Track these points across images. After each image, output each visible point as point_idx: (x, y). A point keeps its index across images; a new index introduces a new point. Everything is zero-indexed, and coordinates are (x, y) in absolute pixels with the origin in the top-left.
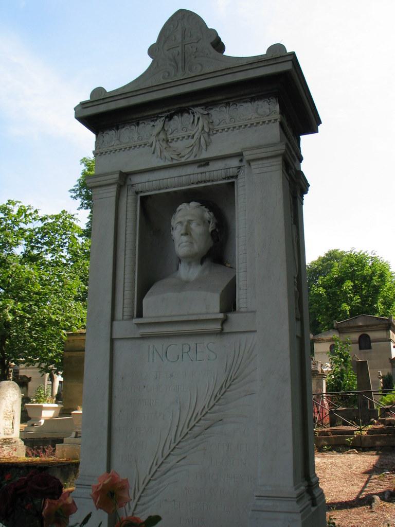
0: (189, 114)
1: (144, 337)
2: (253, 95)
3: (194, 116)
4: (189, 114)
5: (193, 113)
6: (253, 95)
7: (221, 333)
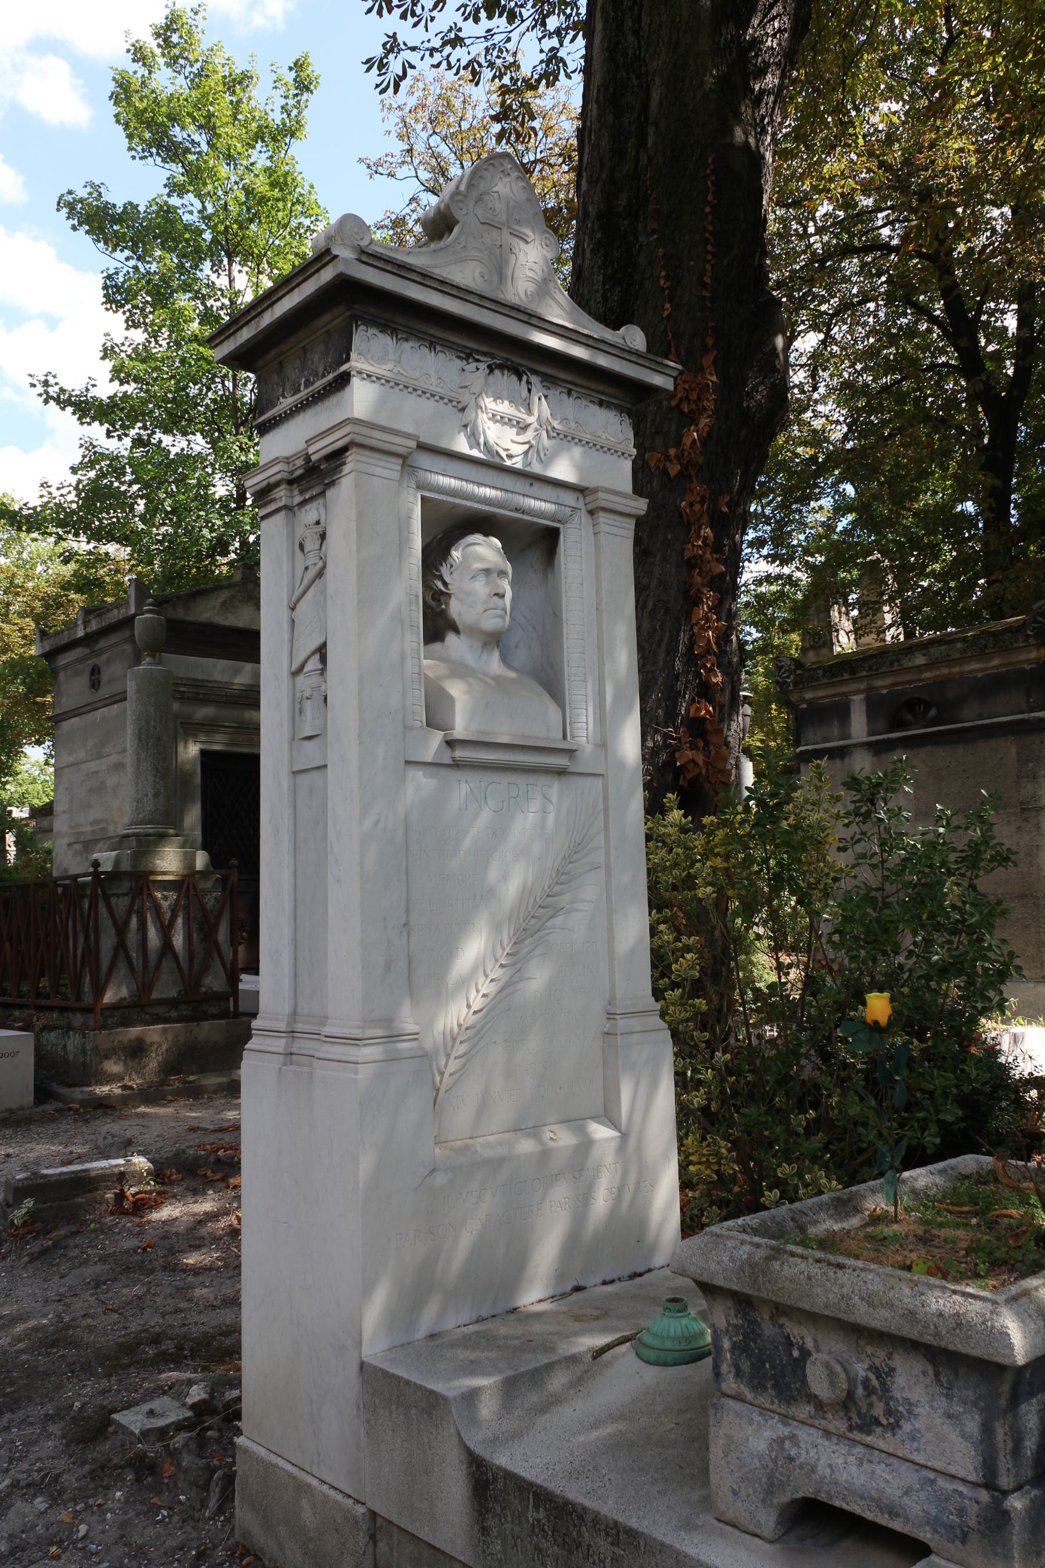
0: (520, 379)
1: (456, 765)
2: (603, 398)
3: (529, 391)
4: (520, 379)
5: (528, 383)
6: (603, 398)
7: (561, 773)
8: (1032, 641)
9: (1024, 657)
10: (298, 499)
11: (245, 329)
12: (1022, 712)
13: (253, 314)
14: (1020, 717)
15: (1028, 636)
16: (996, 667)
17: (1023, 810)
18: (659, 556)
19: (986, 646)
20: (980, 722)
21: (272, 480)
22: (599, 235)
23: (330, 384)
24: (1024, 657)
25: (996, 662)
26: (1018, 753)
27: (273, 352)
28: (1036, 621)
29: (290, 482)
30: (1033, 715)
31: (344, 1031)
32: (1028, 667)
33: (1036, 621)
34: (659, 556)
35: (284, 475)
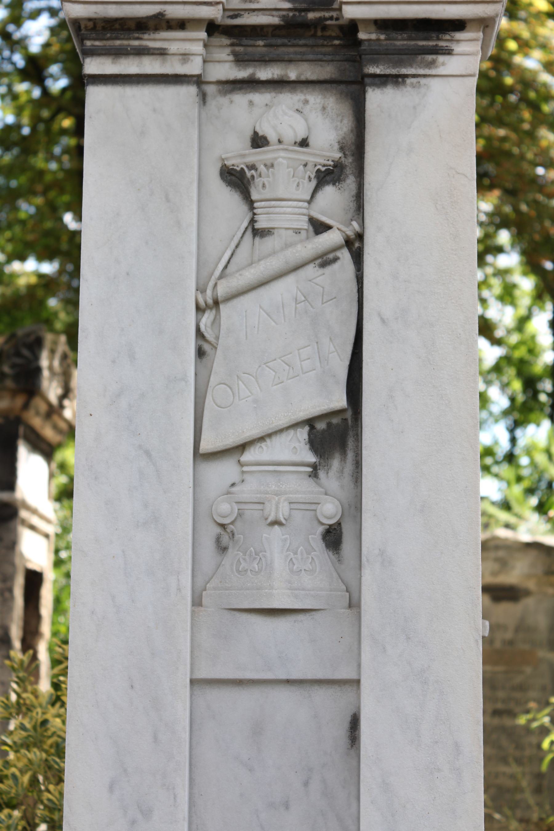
28: (18, 354)
29: (212, 28)
33: (18, 354)
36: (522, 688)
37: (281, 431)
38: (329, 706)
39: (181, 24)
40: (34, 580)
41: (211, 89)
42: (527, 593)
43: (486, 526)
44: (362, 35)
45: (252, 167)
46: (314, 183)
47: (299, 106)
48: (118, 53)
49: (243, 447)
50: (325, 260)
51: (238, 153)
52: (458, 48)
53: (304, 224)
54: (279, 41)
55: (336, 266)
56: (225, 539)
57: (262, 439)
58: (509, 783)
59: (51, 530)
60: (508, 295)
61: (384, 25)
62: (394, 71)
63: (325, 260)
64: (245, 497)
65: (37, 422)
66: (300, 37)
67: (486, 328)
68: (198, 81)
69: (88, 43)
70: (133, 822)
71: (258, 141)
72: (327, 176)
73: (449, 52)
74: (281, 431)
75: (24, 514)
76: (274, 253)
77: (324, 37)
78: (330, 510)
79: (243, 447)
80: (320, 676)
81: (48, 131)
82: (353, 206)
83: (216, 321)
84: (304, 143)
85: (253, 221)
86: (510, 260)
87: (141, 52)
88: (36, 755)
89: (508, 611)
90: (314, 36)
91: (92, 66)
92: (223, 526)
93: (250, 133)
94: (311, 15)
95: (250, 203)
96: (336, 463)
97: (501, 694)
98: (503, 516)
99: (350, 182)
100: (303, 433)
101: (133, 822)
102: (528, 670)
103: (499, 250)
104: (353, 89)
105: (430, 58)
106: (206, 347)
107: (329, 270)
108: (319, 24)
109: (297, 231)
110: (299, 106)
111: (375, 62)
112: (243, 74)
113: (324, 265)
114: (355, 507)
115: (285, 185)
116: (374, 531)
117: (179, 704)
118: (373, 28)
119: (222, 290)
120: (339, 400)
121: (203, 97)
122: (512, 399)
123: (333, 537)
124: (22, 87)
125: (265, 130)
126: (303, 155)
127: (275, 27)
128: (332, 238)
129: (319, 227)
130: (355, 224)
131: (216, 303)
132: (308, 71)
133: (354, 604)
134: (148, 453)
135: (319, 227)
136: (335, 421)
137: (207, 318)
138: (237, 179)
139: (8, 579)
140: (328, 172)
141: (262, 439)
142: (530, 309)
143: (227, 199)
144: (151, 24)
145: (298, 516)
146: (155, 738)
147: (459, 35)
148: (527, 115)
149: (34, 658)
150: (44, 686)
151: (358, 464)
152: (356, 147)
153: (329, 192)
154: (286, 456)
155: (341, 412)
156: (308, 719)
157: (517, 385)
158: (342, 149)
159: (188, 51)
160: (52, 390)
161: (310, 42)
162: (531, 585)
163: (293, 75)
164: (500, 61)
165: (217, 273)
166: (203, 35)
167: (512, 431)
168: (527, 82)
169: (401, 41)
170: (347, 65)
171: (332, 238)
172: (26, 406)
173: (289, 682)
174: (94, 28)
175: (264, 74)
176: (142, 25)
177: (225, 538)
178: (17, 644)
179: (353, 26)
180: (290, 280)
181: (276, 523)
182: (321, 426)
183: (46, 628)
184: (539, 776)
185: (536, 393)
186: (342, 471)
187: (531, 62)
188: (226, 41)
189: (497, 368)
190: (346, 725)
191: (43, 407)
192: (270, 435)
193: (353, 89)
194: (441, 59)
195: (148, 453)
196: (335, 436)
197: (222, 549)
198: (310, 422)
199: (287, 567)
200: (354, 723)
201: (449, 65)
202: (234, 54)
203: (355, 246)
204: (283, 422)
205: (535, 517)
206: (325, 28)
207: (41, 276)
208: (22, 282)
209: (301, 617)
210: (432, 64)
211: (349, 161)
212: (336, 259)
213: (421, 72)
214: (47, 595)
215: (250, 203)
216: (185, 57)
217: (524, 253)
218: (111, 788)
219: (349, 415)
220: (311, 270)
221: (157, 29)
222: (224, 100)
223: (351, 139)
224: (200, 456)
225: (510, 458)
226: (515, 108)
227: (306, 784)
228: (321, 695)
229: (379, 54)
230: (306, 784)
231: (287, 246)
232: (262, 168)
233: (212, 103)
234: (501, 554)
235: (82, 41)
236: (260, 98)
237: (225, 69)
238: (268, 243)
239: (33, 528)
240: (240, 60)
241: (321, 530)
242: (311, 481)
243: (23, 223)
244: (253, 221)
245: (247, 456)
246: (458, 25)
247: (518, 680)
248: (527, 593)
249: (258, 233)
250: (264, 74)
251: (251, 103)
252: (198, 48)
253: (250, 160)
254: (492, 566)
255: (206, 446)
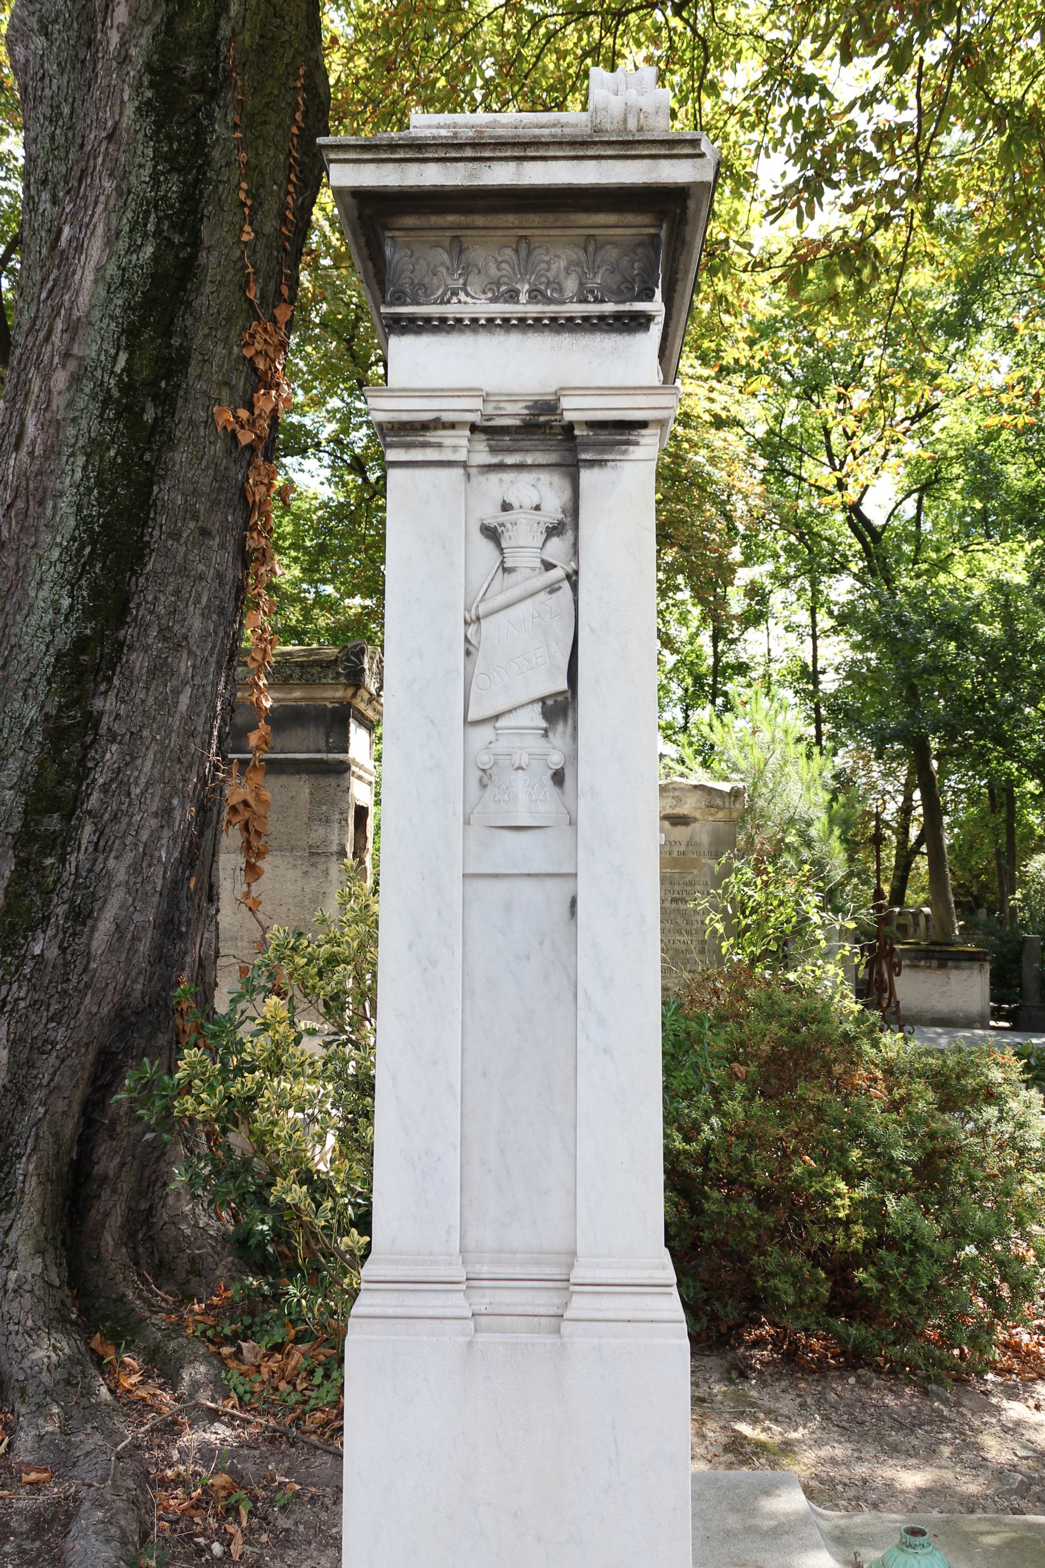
8: (343, 680)
9: (329, 694)
10: (484, 457)
11: (432, 167)
12: (319, 751)
13: (469, 153)
14: (318, 756)
15: (338, 673)
16: (295, 700)
17: (312, 854)
18: (217, 540)
19: (291, 676)
20: (273, 756)
21: (447, 417)
22: (149, 94)
23: (602, 318)
24: (329, 694)
25: (297, 694)
26: (311, 793)
27: (451, 219)
28: (349, 660)
29: (474, 428)
30: (332, 756)
31: (511, 1270)
32: (330, 706)
33: (349, 660)
34: (217, 540)
35: (475, 418)
36: (691, 884)
37: (523, 706)
38: (558, 891)
39: (453, 426)
40: (361, 813)
41: (473, 471)
42: (695, 820)
43: (668, 776)
44: (577, 432)
45: (502, 525)
46: (545, 535)
47: (534, 482)
48: (409, 446)
49: (497, 717)
50: (552, 589)
51: (492, 515)
52: (643, 441)
53: (539, 565)
54: (520, 437)
55: (560, 593)
56: (486, 779)
57: (510, 711)
58: (683, 947)
59: (372, 779)
60: (683, 620)
61: (592, 425)
62: (599, 457)
63: (552, 589)
64: (499, 751)
65: (362, 706)
66: (535, 434)
67: (667, 641)
68: (464, 465)
69: (388, 439)
70: (425, 970)
71: (506, 507)
72: (554, 531)
73: (637, 444)
74: (523, 706)
75: (353, 768)
76: (517, 584)
77: (551, 434)
78: (556, 760)
79: (497, 717)
80: (551, 871)
81: (368, 507)
82: (571, 551)
83: (478, 631)
84: (537, 508)
85: (503, 562)
86: (685, 595)
87: (425, 445)
88: (362, 928)
89: (681, 833)
90: (544, 433)
91: (392, 455)
92: (484, 771)
93: (500, 502)
94: (542, 419)
95: (501, 550)
96: (560, 727)
97: (677, 888)
98: (680, 768)
99: (569, 535)
100: (538, 707)
101: (425, 970)
102: (695, 871)
103: (677, 588)
104: (571, 469)
105: (624, 447)
106: (471, 649)
107: (555, 595)
108: (547, 425)
109: (533, 569)
110: (534, 482)
111: (585, 451)
112: (495, 460)
113: (551, 592)
114: (573, 757)
115: (525, 537)
116: (586, 773)
117: (455, 890)
118: (584, 427)
119: (481, 611)
120: (563, 685)
121: (468, 476)
122: (686, 690)
123: (558, 778)
124: (349, 478)
125: (511, 499)
126: (536, 516)
127: (518, 427)
128: (557, 573)
129: (548, 566)
130: (573, 564)
131: (478, 619)
132: (540, 458)
133: (573, 823)
134: (432, 722)
135: (548, 566)
136: (560, 699)
137: (472, 629)
138: (492, 533)
139: (343, 812)
140: (554, 528)
141: (510, 711)
142: (698, 628)
143: (486, 547)
144: (432, 425)
145: (534, 763)
146: (440, 914)
147: (643, 432)
148: (696, 493)
149: (362, 862)
150: (369, 883)
151: (575, 728)
152: (574, 510)
153: (555, 541)
154: (527, 723)
155: (564, 692)
156: (541, 901)
157: (689, 681)
158: (563, 512)
159: (457, 444)
160: (372, 685)
161: (542, 437)
162: (698, 815)
163: (529, 461)
164: (678, 458)
165: (479, 598)
166: (468, 433)
167: (686, 711)
168: (697, 472)
169: (604, 436)
170: (567, 453)
171: (557, 573)
172: (354, 695)
173: (529, 875)
174: (392, 429)
175: (510, 460)
176: (425, 426)
177: (485, 778)
178: (350, 855)
179: (570, 426)
180: (529, 602)
181: (520, 768)
182: (550, 702)
183: (370, 845)
184: (703, 942)
185: (702, 687)
186: (564, 733)
187: (700, 457)
188: (483, 437)
189: (675, 669)
190: (568, 904)
191: (366, 696)
192: (515, 709)
193: (571, 469)
194: (631, 448)
195: (432, 722)
196: (559, 709)
197: (484, 786)
198: (543, 700)
199: (527, 797)
200: (574, 902)
201: (635, 452)
202: (489, 446)
203: (573, 579)
204: (525, 699)
205: (701, 770)
206: (551, 427)
207: (364, 608)
208: (352, 612)
209: (537, 831)
210: (625, 452)
211: (568, 520)
212: (560, 588)
213: (618, 457)
214: (371, 823)
215: (501, 550)
216: (455, 448)
217: (692, 589)
218: (410, 947)
219: (569, 695)
220: (543, 596)
221: (435, 429)
222: (482, 479)
223: (570, 505)
224: (468, 723)
225: (685, 729)
226: (688, 490)
227: (541, 943)
228: (551, 884)
229: (589, 445)
230: (541, 943)
231: (526, 579)
232: (509, 525)
233: (474, 480)
234: (677, 793)
235: (384, 438)
236: (507, 477)
237: (484, 457)
238: (513, 577)
239: (360, 778)
240: (493, 450)
241: (550, 772)
242: (543, 740)
243: (352, 571)
244: (503, 562)
245: (500, 723)
246: (643, 424)
247: (689, 878)
248: (695, 820)
249: (506, 570)
250: (510, 460)
251: (501, 480)
252: (464, 442)
253: (500, 520)
254: (669, 801)
255: (471, 717)
